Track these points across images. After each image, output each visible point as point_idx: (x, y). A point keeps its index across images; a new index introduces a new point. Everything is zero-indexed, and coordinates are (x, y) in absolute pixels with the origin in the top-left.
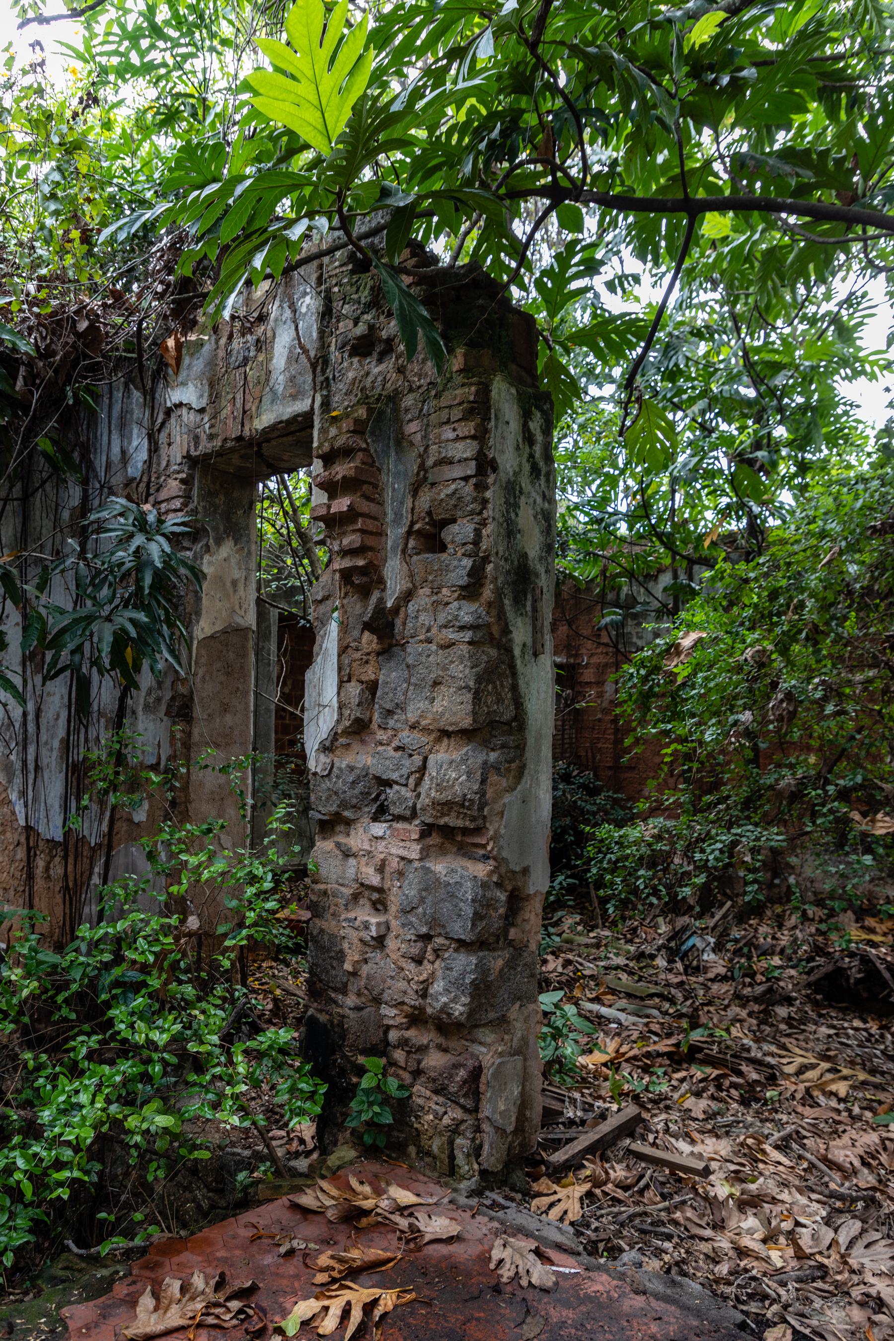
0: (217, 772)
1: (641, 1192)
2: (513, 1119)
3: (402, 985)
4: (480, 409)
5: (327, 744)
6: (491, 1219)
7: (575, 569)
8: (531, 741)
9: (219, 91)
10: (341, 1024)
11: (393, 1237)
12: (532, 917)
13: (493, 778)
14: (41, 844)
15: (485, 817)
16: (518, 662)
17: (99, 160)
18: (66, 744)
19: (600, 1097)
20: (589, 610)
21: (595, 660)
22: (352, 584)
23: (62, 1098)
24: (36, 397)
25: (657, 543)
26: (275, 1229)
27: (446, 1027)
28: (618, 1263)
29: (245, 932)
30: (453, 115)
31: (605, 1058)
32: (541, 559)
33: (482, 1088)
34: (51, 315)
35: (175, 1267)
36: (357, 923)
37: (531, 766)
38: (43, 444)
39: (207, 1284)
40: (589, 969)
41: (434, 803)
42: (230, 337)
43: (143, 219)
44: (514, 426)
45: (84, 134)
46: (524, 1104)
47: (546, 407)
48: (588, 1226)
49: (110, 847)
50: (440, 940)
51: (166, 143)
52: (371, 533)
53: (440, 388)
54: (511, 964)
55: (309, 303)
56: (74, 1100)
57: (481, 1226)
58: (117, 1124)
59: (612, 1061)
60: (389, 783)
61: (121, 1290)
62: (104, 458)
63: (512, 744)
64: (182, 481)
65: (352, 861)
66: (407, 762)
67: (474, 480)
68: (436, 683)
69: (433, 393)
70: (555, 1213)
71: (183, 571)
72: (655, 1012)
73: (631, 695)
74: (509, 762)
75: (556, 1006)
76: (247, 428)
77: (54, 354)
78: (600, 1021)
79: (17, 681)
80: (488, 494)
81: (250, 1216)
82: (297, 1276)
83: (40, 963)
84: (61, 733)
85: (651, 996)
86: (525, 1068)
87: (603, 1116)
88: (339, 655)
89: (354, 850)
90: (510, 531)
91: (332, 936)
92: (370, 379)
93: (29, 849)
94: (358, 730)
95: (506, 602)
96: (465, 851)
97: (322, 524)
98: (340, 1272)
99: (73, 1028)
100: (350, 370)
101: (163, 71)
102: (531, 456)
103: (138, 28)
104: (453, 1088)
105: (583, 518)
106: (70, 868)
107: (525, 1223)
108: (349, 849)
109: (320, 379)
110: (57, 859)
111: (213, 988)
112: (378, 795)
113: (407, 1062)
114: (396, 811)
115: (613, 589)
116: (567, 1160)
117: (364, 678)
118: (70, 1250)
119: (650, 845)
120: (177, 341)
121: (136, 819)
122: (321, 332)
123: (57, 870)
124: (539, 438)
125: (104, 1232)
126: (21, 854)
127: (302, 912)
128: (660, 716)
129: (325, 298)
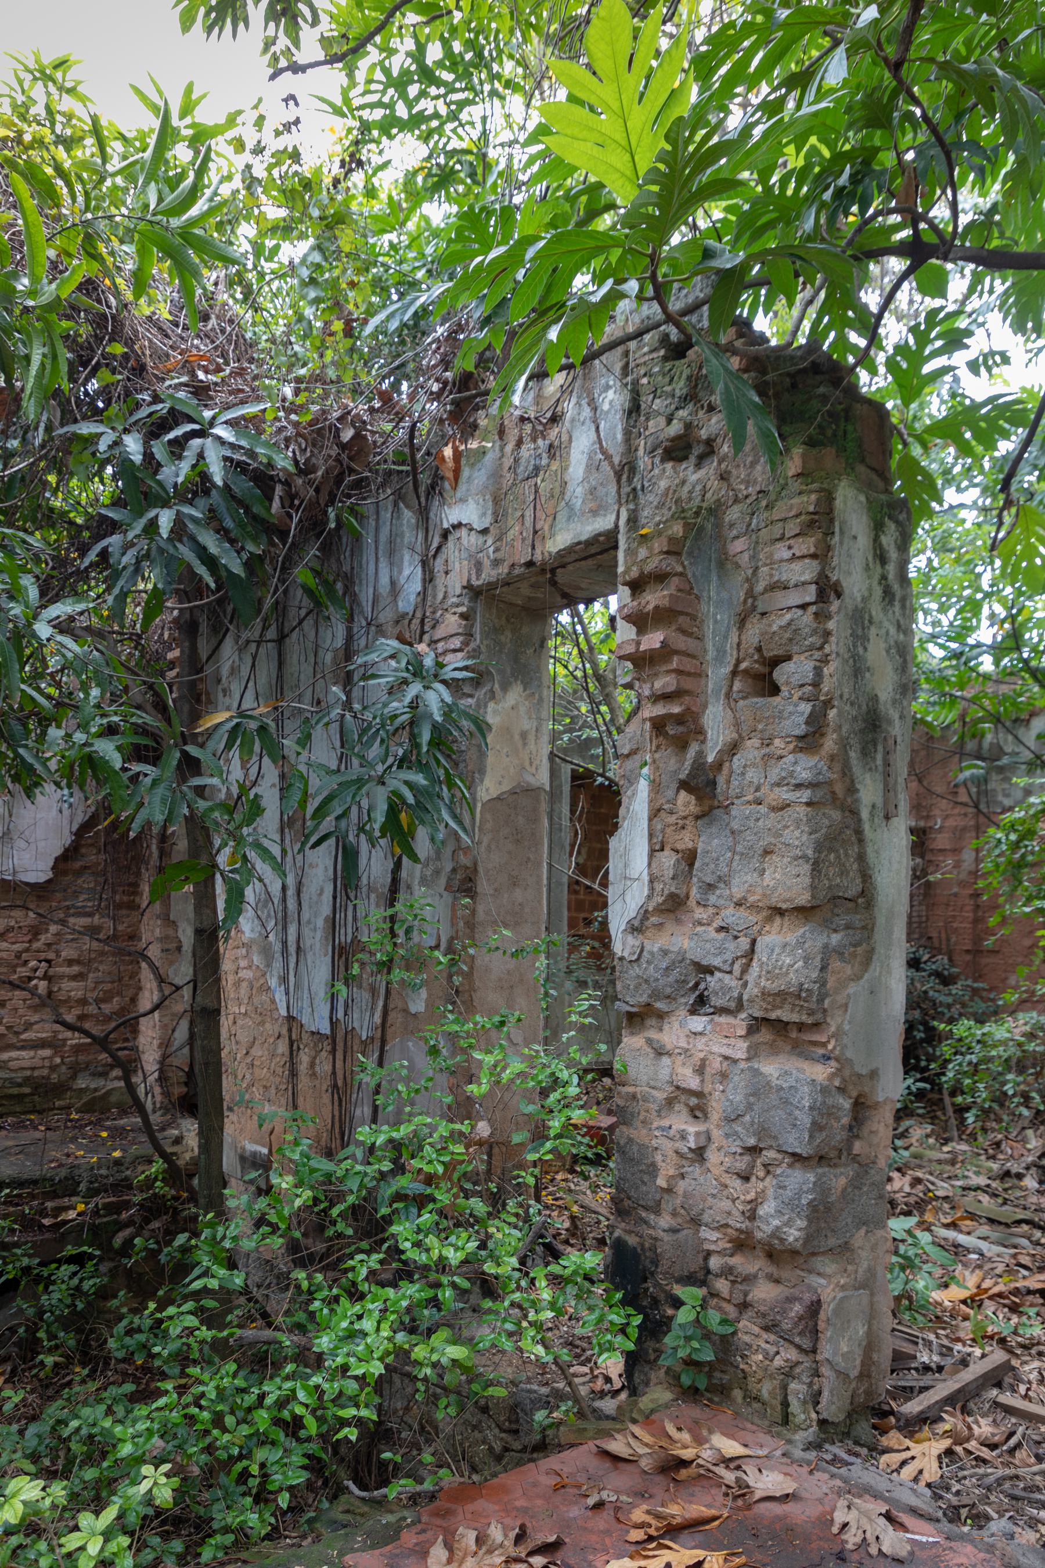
0: (507, 958)
1: (1012, 1451)
2: (858, 1362)
3: (726, 1205)
4: (822, 521)
5: (636, 923)
6: (833, 1476)
7: (928, 713)
8: (881, 921)
9: (502, 145)
10: (653, 1249)
11: (718, 1493)
12: (882, 1128)
13: (836, 964)
14: (305, 1036)
15: (825, 1011)
16: (866, 826)
17: (365, 236)
18: (332, 923)
19: (958, 1340)
20: (944, 761)
21: (950, 823)
22: (666, 735)
23: (344, 1324)
24: (295, 520)
25: (1030, 681)
26: (581, 1478)
27: (776, 1254)
28: (984, 1533)
29: (549, 1145)
30: (794, 159)
31: (964, 1294)
32: (894, 702)
33: (821, 1325)
34: (311, 424)
35: (469, 1516)
36: (672, 1132)
37: (880, 950)
38: (302, 574)
39: (506, 1536)
40: (943, 1189)
41: (765, 994)
42: (519, 443)
43: (418, 303)
44: (863, 541)
45: (346, 203)
46: (870, 1347)
47: (902, 517)
48: (948, 1489)
49: (383, 1042)
50: (770, 1154)
51: (438, 212)
52: (689, 674)
53: (773, 497)
54: (856, 1183)
55: (612, 399)
56: (357, 1326)
57: (821, 1484)
58: (403, 1354)
59: (972, 1298)
60: (709, 970)
61: (409, 1538)
62: (371, 591)
63: (858, 924)
64: (463, 616)
65: (666, 1061)
66: (731, 945)
67: (813, 609)
68: (767, 852)
69: (764, 503)
70: (908, 1472)
71: (465, 724)
72: (1024, 1242)
73: (997, 865)
74: (855, 946)
75: (909, 1232)
76: (538, 551)
77: (313, 469)
78: (957, 1250)
79: (276, 850)
80: (831, 625)
81: (553, 1462)
82: (608, 1532)
83: (313, 1171)
84: (326, 910)
85: (1019, 1222)
86: (872, 1304)
87: (964, 1362)
88: (650, 820)
89: (669, 1047)
90: (858, 669)
91: (643, 1147)
92: (686, 488)
93: (291, 1043)
94: (674, 906)
95: (852, 754)
96: (799, 1049)
97: (629, 665)
98: (657, 1529)
99: (349, 1245)
100: (662, 478)
101: (435, 123)
102: (884, 577)
103: (405, 73)
104: (786, 1325)
105: (940, 653)
106: (339, 1064)
107: (872, 1482)
108: (663, 1047)
109: (626, 489)
110: (324, 1054)
111: (504, 1205)
112: (697, 984)
113: (731, 1293)
114: (717, 1001)
115: (974, 736)
116: (922, 1412)
117: (680, 846)
118: (350, 1492)
119: (1020, 1045)
120: (455, 449)
121: (413, 1009)
122: (628, 434)
123: (324, 1067)
124: (893, 555)
125: (385, 1475)
126: (282, 1047)
127: (603, 1117)
128: (1033, 889)
129: (632, 391)
